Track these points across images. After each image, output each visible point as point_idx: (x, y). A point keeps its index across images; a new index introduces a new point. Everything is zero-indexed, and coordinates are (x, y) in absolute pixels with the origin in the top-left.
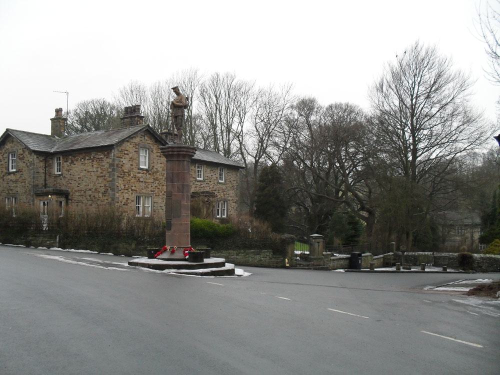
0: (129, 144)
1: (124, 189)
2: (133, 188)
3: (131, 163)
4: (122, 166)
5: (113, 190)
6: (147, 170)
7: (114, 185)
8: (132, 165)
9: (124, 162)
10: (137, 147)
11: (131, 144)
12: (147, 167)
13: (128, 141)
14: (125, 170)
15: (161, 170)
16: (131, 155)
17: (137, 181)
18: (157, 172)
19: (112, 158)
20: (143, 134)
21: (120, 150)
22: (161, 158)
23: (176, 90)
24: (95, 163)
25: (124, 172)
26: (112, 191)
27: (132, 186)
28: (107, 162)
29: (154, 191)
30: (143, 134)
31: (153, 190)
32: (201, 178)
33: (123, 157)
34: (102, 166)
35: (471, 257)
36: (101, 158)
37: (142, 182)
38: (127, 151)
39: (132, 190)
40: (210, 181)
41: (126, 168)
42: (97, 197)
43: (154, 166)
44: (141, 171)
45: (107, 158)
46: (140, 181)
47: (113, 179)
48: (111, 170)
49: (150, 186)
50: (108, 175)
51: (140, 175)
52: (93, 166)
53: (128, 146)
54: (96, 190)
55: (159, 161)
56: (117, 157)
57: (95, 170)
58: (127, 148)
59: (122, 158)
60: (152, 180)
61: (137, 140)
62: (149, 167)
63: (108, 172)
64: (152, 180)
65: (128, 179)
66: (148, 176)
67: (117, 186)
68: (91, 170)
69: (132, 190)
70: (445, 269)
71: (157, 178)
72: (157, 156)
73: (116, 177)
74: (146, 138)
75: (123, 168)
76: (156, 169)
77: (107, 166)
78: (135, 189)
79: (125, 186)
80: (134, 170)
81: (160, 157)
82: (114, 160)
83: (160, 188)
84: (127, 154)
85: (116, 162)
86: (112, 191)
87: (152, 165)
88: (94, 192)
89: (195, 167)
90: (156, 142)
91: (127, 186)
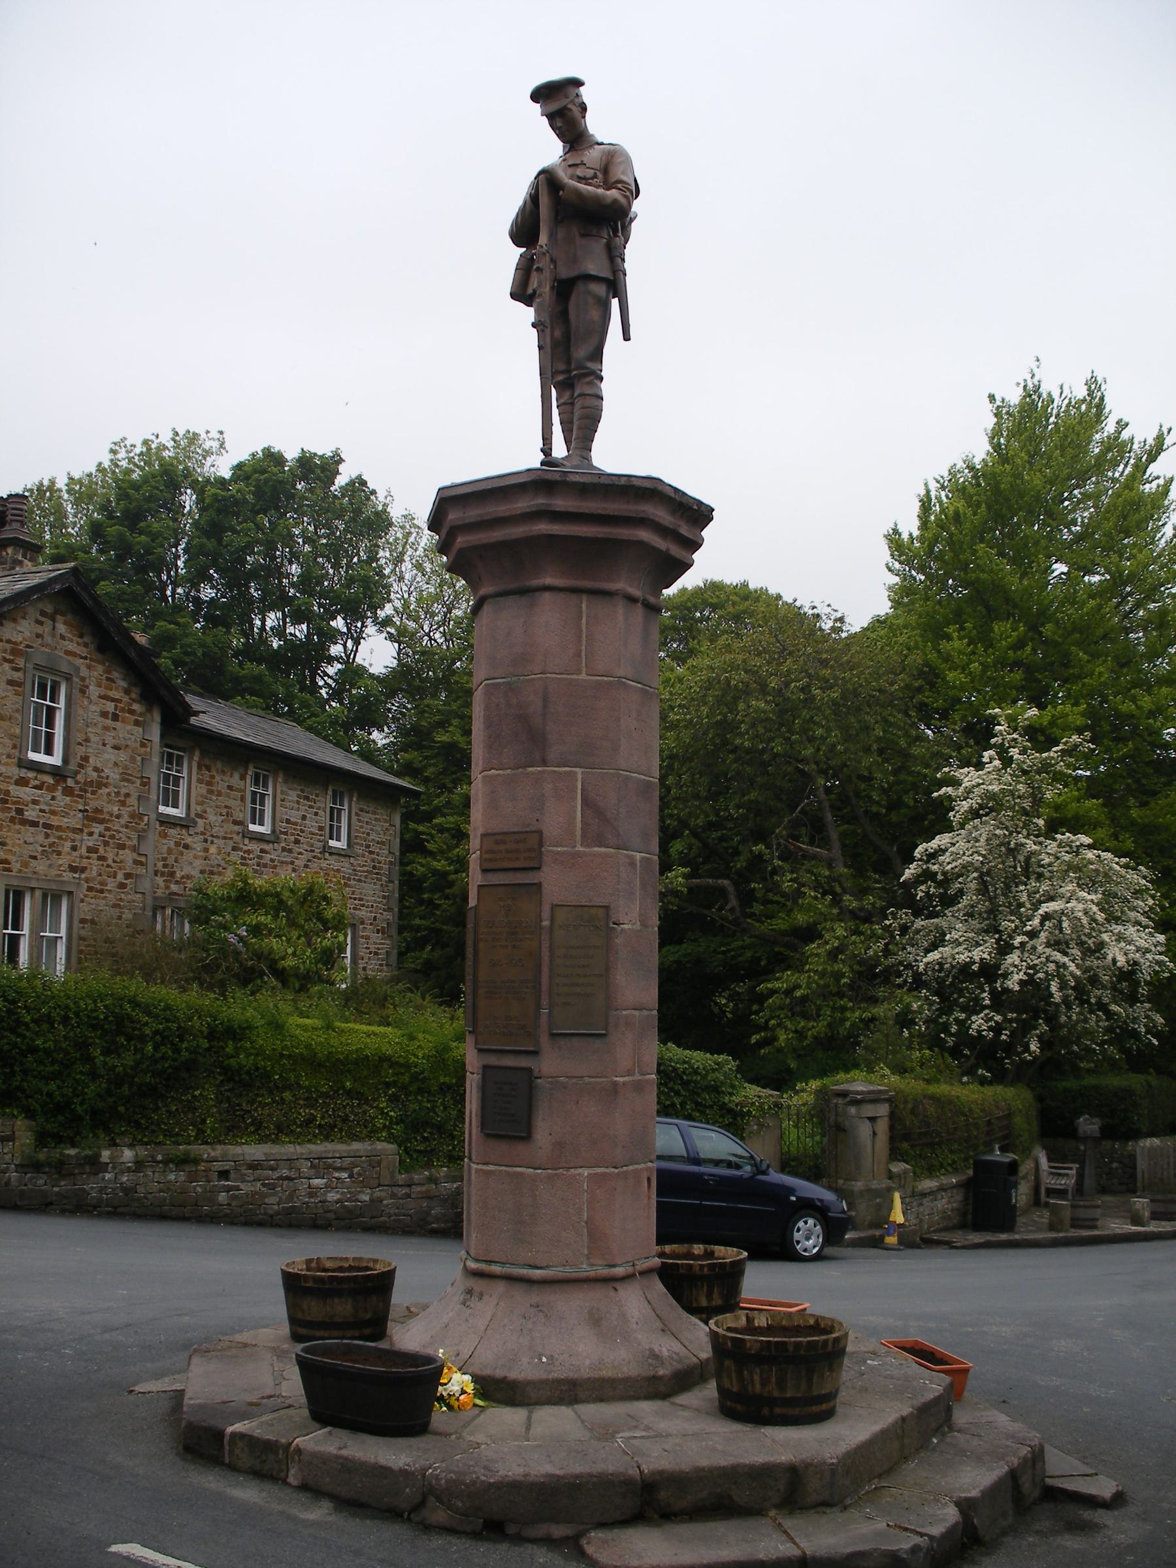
10: (21, 662)
15: (114, 775)
17: (12, 820)
18: (100, 785)
22: (118, 725)
23: (560, 102)
29: (83, 870)
30: (49, 609)
37: (34, 824)
40: (297, 842)
43: (86, 759)
44: (31, 775)
46: (24, 822)
49: (68, 844)
51: (26, 793)
60: (75, 820)
64: (75, 820)
66: (62, 800)
71: (97, 810)
72: (104, 714)
74: (62, 628)
76: (96, 769)
81: (115, 717)
83: (110, 856)
87: (81, 751)
89: (243, 778)
90: (101, 649)
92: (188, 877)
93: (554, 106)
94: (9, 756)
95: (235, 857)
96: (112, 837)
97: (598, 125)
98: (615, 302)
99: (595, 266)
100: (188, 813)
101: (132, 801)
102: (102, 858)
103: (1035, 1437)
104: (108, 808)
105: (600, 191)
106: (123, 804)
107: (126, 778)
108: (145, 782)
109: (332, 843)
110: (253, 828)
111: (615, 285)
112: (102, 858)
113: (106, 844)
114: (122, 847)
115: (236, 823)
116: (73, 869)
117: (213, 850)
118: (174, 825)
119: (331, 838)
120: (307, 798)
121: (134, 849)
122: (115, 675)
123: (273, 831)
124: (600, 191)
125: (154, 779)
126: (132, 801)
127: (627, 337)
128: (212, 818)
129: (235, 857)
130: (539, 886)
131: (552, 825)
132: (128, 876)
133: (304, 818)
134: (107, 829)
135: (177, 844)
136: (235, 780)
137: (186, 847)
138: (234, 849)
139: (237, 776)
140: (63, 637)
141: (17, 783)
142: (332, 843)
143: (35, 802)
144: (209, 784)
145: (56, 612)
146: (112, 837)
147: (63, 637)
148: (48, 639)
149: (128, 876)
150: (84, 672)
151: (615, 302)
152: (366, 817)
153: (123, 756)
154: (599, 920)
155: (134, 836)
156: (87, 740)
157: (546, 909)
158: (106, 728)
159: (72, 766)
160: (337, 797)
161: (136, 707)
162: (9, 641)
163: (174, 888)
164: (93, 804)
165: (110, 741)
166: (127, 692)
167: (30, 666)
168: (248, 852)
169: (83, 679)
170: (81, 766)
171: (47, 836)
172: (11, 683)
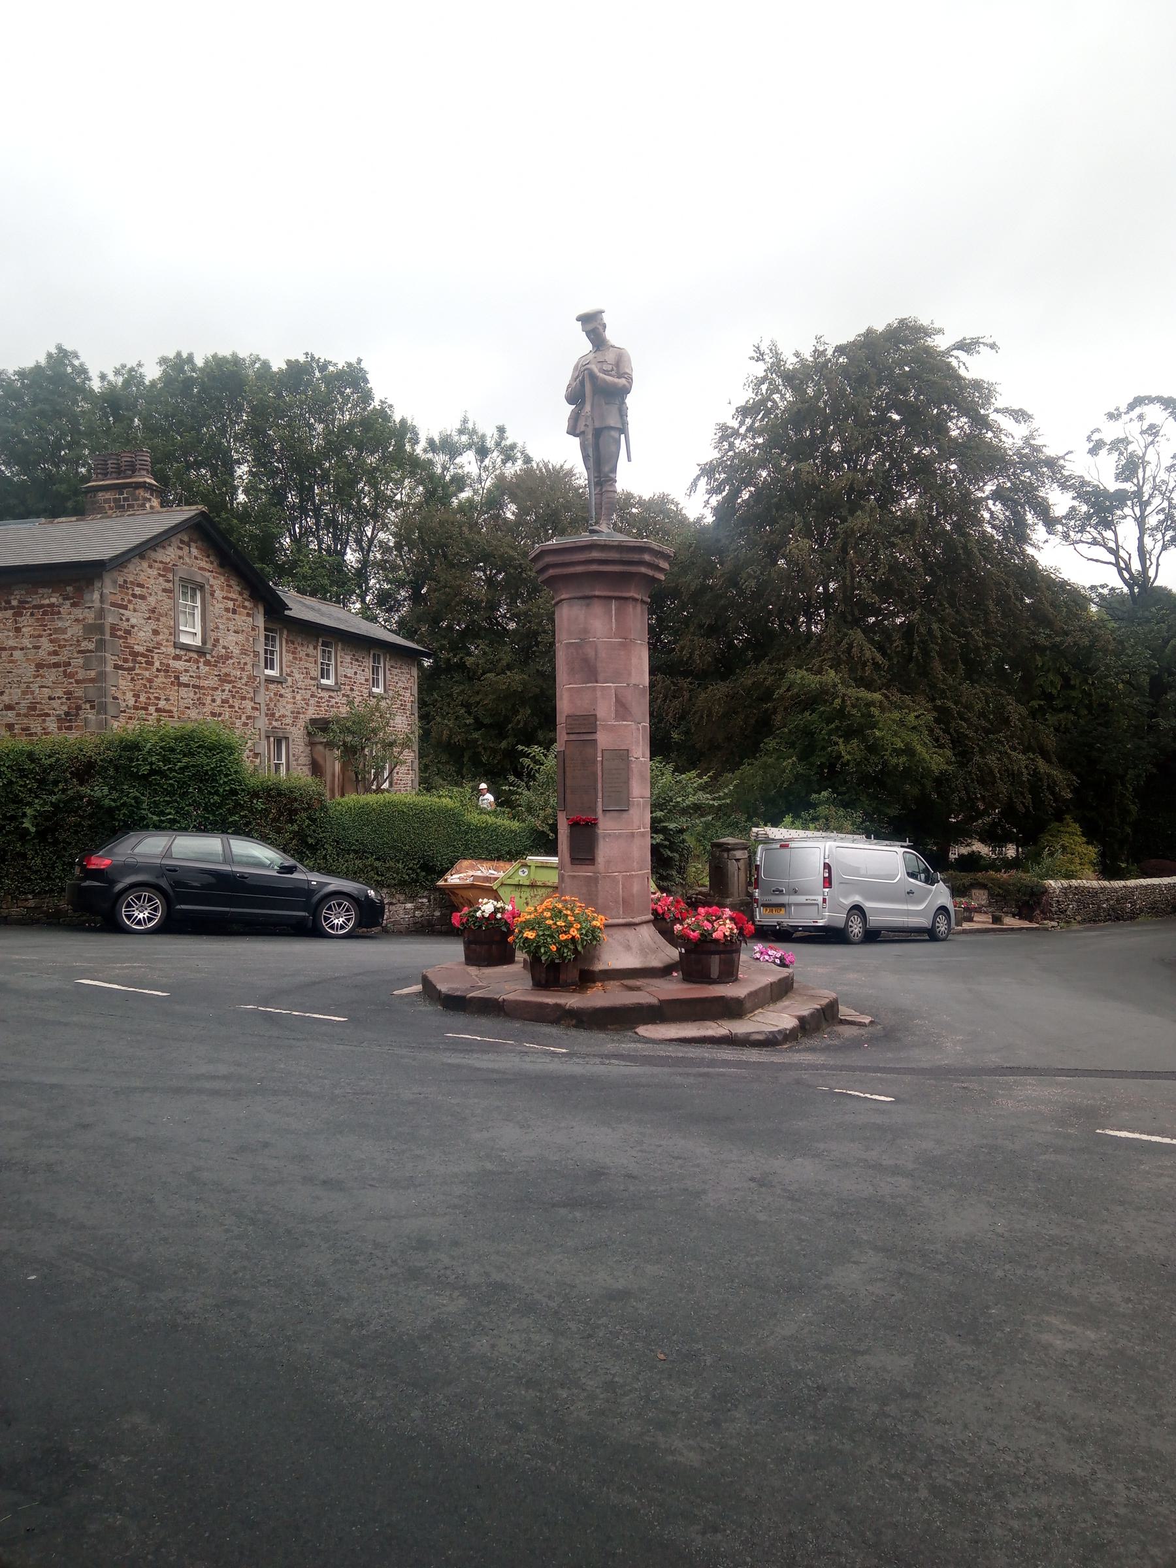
0: (145, 565)
1: (136, 708)
2: (162, 704)
3: (153, 625)
4: (128, 632)
5: (102, 708)
6: (201, 652)
7: (103, 692)
8: (156, 632)
9: (133, 621)
10: (170, 576)
11: (150, 567)
12: (197, 642)
13: (142, 557)
14: (137, 648)
15: (236, 651)
16: (152, 600)
17: (172, 683)
18: (228, 657)
19: (97, 604)
20: (186, 539)
21: (120, 581)
22: (236, 617)
23: (592, 324)
24: (26, 621)
25: (136, 655)
26: (99, 713)
27: (158, 699)
28: (76, 620)
29: (220, 715)
30: (186, 539)
31: (217, 710)
32: (328, 678)
33: (131, 607)
34: (57, 631)
35: (1045, 891)
36: (52, 605)
37: (187, 686)
38: (141, 586)
39: (158, 710)
40: (352, 690)
41: (142, 638)
42: (39, 730)
43: (217, 640)
44: (182, 653)
45: (74, 605)
46: (180, 685)
47: (102, 676)
48: (92, 646)
49: (209, 698)
50: (81, 661)
51: (179, 665)
52: (18, 630)
53: (145, 573)
54: (34, 709)
55: (231, 625)
56: (113, 605)
57: (26, 642)
58: (142, 578)
59: (125, 607)
60: (212, 682)
61: (169, 554)
62: (204, 642)
63: (79, 652)
64: (212, 682)
65: (147, 674)
66: (204, 669)
67: (115, 698)
68: (11, 643)
69: (158, 710)
70: (997, 920)
71: (226, 675)
72: (227, 610)
73: (109, 669)
74: (195, 552)
75: (131, 641)
76: (224, 647)
77: (76, 630)
78: (167, 708)
79: (137, 696)
80: (164, 649)
81: (234, 612)
82: (101, 614)
83: (237, 705)
84: (143, 597)
85: (110, 620)
86: (99, 713)
87: (213, 635)
88: (26, 716)
89: (315, 648)
90: (221, 565)
91: (143, 699)
92: (284, 716)
93: (590, 327)
94: (167, 641)
95: (312, 701)
96: (237, 692)
97: (612, 335)
98: (623, 436)
99: (613, 421)
100: (281, 674)
101: (249, 667)
102: (231, 707)
103: (834, 995)
104: (234, 673)
105: (616, 380)
106: (243, 669)
107: (244, 652)
108: (256, 654)
109: (375, 690)
110: (324, 681)
111: (623, 430)
112: (231, 707)
113: (234, 697)
114: (244, 698)
115: (312, 678)
116: (213, 714)
117: (298, 697)
118: (273, 682)
119: (323, 677)
120: (357, 660)
121: (252, 699)
122: (232, 583)
123: (336, 683)
124: (616, 380)
125: (262, 652)
126: (249, 667)
127: (629, 460)
128: (297, 676)
129: (312, 701)
130: (595, 740)
131: (601, 713)
132: (249, 718)
133: (356, 673)
134: (234, 687)
135: (275, 694)
136: (311, 650)
137: (281, 696)
138: (312, 696)
139: (311, 647)
140: (196, 558)
141: (174, 658)
142: (375, 690)
143: (186, 671)
144: (294, 653)
145: (191, 540)
146: (237, 692)
147: (196, 558)
148: (187, 560)
149: (249, 718)
150: (212, 581)
151: (623, 436)
152: (395, 671)
153: (241, 638)
154: (623, 756)
155: (251, 690)
156: (217, 628)
157: (599, 754)
158: (229, 619)
159: (209, 646)
160: (376, 659)
161: (247, 604)
162: (161, 562)
163: (275, 724)
164: (224, 671)
165: (232, 628)
166: (241, 594)
167: (177, 579)
168: (321, 698)
169: (212, 586)
170: (214, 646)
171: (195, 693)
172: (164, 590)
